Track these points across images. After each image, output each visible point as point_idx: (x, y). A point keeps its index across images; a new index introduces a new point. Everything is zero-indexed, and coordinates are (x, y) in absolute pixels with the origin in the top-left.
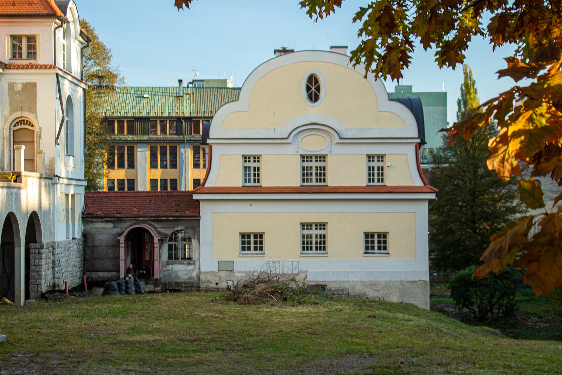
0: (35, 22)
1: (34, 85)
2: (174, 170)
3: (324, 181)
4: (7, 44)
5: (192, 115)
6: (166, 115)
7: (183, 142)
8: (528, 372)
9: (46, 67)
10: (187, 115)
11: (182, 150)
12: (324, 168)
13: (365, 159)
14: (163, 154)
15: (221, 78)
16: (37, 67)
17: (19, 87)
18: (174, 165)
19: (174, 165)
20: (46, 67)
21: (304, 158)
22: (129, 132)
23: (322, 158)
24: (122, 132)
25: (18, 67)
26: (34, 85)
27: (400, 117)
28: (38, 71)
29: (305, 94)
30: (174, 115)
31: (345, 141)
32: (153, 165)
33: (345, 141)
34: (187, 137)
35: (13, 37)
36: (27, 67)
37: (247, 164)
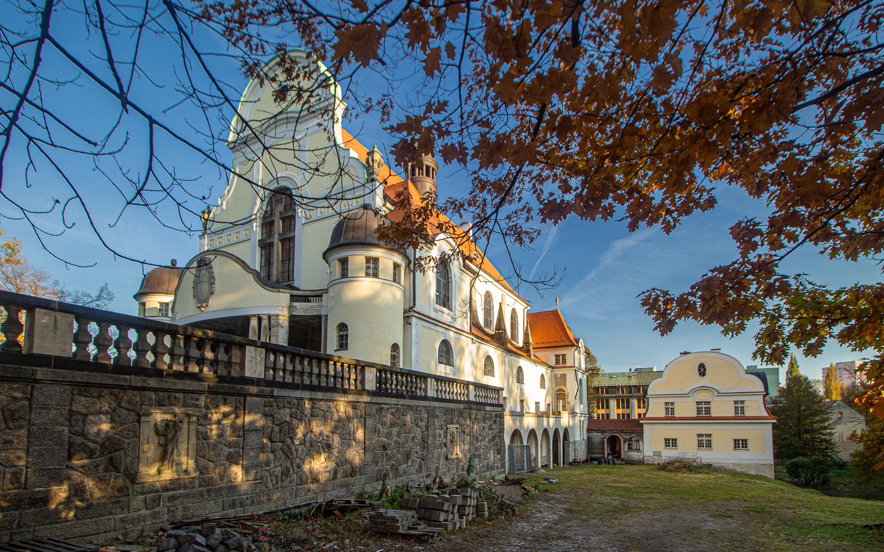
4: (554, 358)
13: (733, 403)
16: (568, 367)
17: (559, 376)
18: (628, 407)
19: (628, 407)
23: (709, 403)
29: (698, 373)
31: (720, 394)
33: (720, 394)
34: (634, 395)
35: (556, 355)
36: (562, 367)
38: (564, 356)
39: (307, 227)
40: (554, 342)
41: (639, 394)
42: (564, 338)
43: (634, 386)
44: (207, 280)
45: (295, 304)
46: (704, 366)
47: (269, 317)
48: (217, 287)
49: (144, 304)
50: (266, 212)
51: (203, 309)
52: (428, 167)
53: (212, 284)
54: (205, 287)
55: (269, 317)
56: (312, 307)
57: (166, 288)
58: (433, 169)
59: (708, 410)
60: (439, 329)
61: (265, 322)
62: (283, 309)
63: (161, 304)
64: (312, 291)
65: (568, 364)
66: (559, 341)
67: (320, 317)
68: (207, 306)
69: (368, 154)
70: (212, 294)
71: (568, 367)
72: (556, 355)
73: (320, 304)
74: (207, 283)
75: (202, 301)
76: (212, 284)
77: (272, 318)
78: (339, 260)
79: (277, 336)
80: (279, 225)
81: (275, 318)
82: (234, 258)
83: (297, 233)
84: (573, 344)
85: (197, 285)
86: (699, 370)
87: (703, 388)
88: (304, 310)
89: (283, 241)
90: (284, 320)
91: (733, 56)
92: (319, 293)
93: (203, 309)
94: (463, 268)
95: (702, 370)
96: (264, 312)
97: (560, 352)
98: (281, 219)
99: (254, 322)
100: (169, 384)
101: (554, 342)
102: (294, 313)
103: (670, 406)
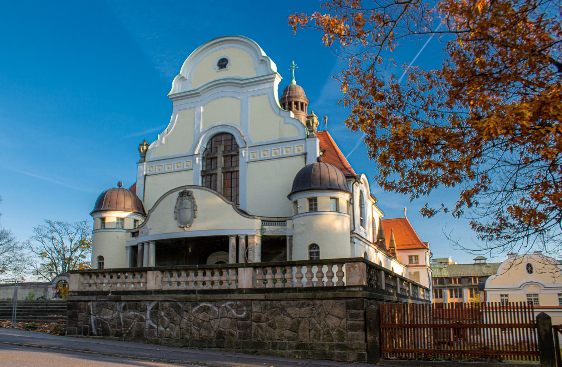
0: (245, 217)
1: (418, 273)
2: (441, 299)
3: (538, 304)
4: (407, 259)
5: (448, 276)
6: (437, 276)
7: (445, 287)
8: (466, 95)
9: (423, 266)
10: (446, 276)
11: (445, 291)
12: (538, 299)
13: (557, 295)
14: (456, 292)
15: (446, 257)
16: (420, 266)
17: (413, 273)
18: (441, 297)
19: (441, 297)
20: (423, 266)
21: (528, 295)
22: (439, 284)
23: (537, 295)
24: (436, 284)
25: (412, 266)
26: (418, 273)
27: (235, 128)
28: (420, 267)
29: (526, 271)
30: (440, 276)
31: (546, 288)
32: (451, 297)
33: (546, 288)
34: (447, 285)
35: (409, 256)
36: (415, 266)
37: (502, 298)
38: (416, 257)
39: (250, 165)
40: (407, 245)
41: (451, 285)
42: (415, 242)
43: (446, 278)
44: (190, 207)
45: (265, 227)
46: (531, 266)
47: (247, 237)
48: (199, 214)
49: (103, 219)
50: (206, 149)
51: (186, 229)
52: (302, 104)
53: (194, 210)
54: (188, 214)
55: (247, 237)
56: (278, 229)
57: (123, 206)
58: (306, 105)
59: (537, 301)
60: (362, 243)
61: (243, 241)
62: (257, 231)
63: (118, 219)
64: (278, 218)
65: (420, 264)
66: (412, 245)
67: (285, 237)
68: (190, 226)
69: (308, 117)
70: (195, 217)
71: (420, 266)
72: (409, 256)
73: (284, 227)
74: (190, 210)
75: (184, 223)
76: (194, 210)
77: (249, 237)
78: (308, 199)
79: (254, 250)
80: (221, 161)
81: (252, 237)
82: (195, 187)
83: (241, 168)
84: (424, 247)
85: (179, 210)
86: (527, 269)
87: (531, 283)
88: (272, 231)
89: (225, 173)
90: (257, 241)
91: (509, 3)
92: (284, 219)
93: (186, 229)
94: (370, 197)
95: (530, 269)
96: (242, 234)
97: (413, 253)
98: (223, 156)
99: (233, 241)
100: (119, 285)
101: (407, 245)
102: (265, 234)
103: (504, 298)
